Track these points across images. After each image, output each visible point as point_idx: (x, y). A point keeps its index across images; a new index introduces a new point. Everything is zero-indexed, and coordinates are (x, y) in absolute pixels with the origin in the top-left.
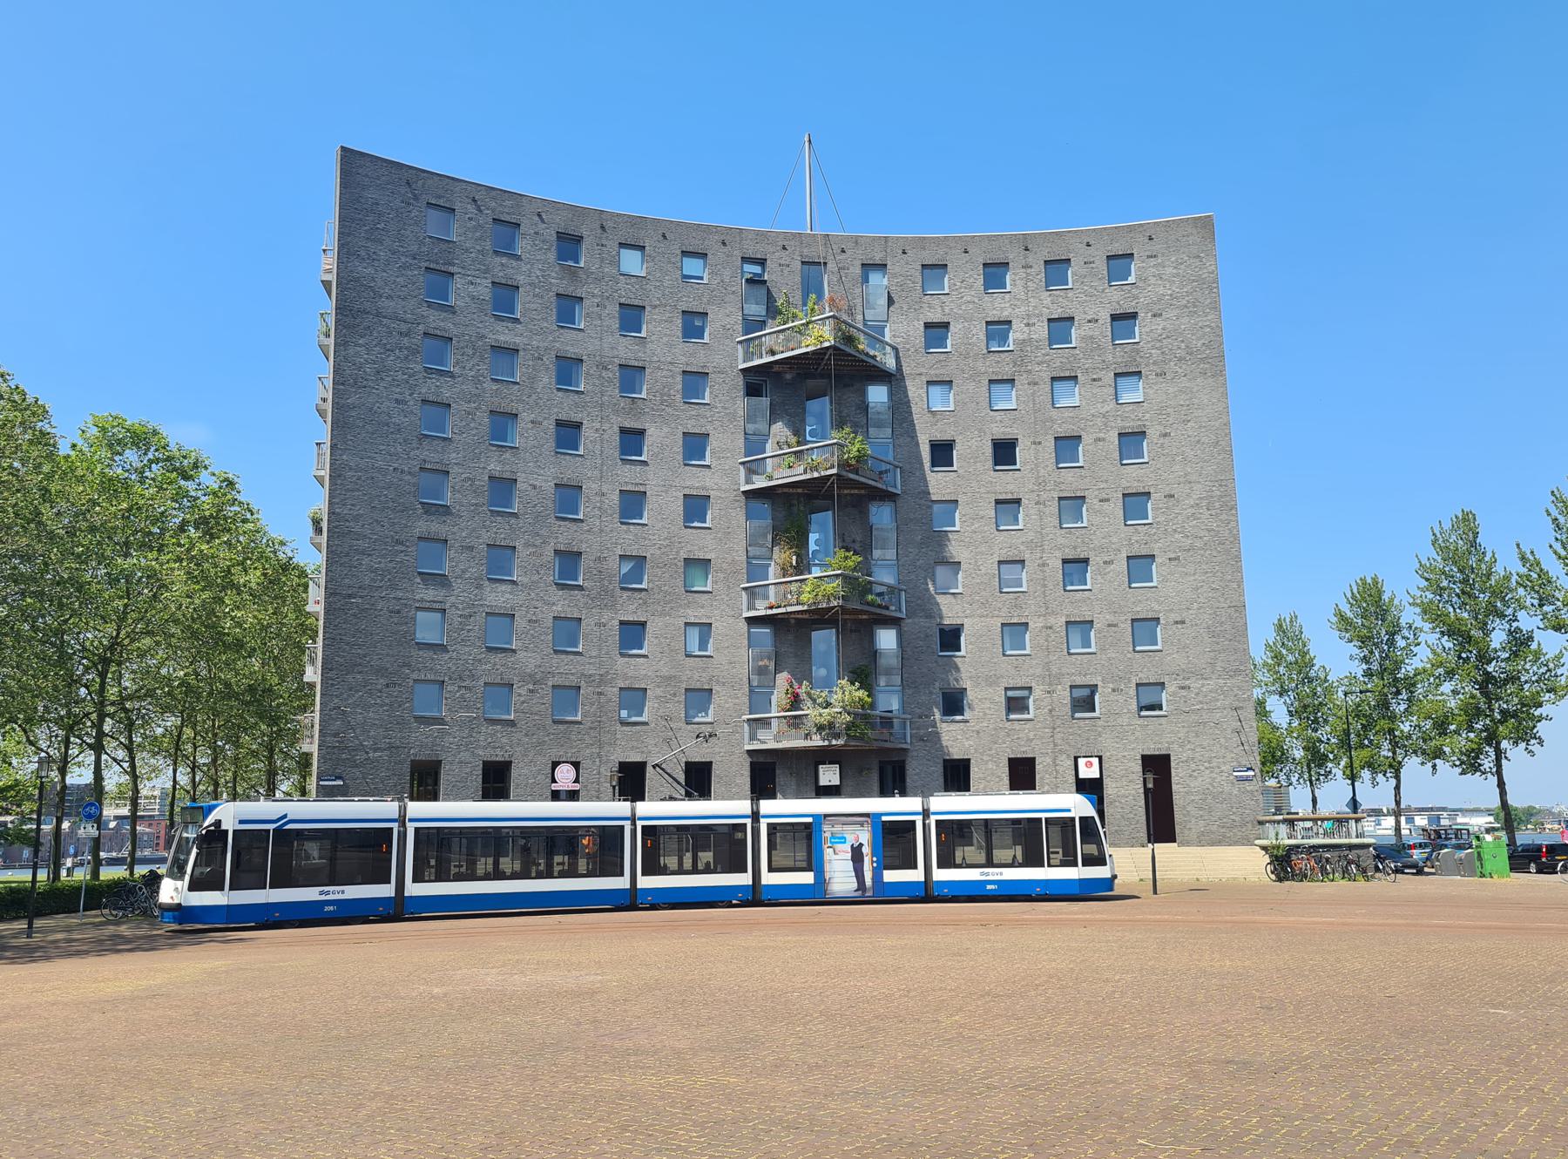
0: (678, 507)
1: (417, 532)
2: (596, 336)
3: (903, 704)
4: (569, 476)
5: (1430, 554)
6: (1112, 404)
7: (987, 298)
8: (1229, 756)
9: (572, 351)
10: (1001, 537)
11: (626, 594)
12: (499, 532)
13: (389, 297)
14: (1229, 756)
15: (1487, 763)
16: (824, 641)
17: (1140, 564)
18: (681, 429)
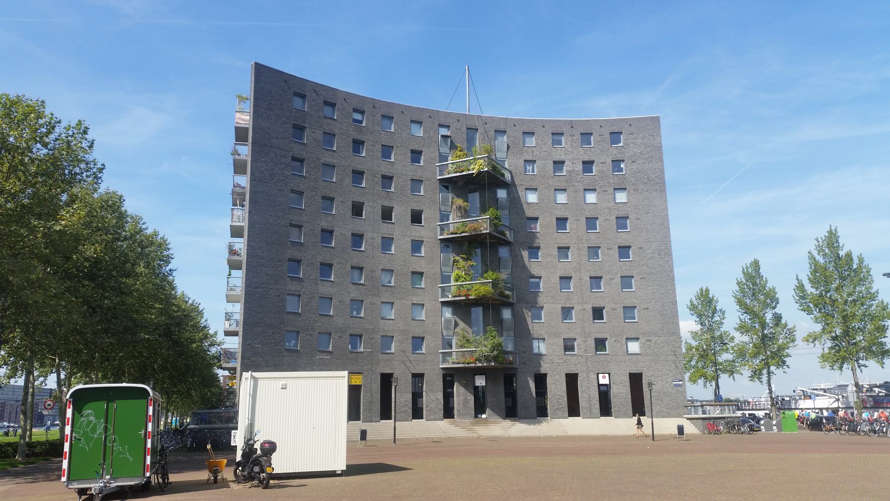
0: (409, 246)
1: (288, 256)
2: (367, 158)
3: (515, 346)
4: (358, 229)
5: (741, 277)
6: (613, 203)
7: (553, 150)
8: (671, 374)
9: (359, 168)
10: (560, 265)
11: (384, 288)
12: (325, 257)
13: (276, 138)
14: (671, 374)
15: (765, 378)
16: (478, 313)
17: (626, 281)
18: (410, 208)
